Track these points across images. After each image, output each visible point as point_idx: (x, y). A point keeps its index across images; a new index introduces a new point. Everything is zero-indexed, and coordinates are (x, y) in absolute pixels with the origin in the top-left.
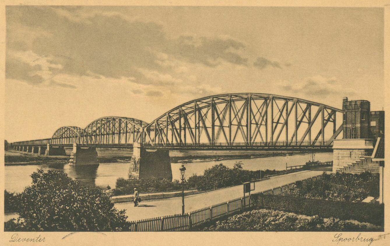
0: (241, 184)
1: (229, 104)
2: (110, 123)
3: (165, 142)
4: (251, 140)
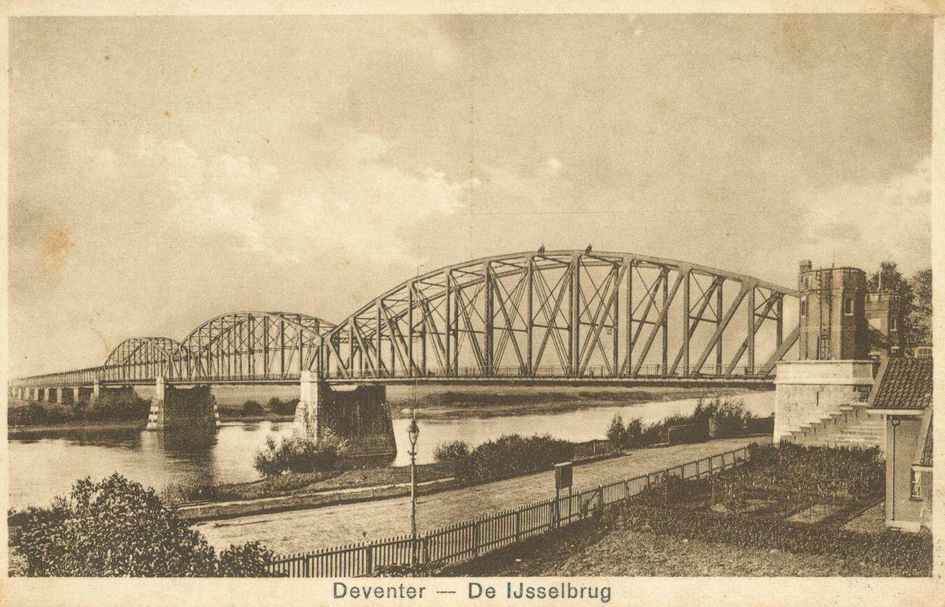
0: (549, 470)
1: (528, 276)
2: (243, 326)
3: (376, 367)
4: (578, 364)
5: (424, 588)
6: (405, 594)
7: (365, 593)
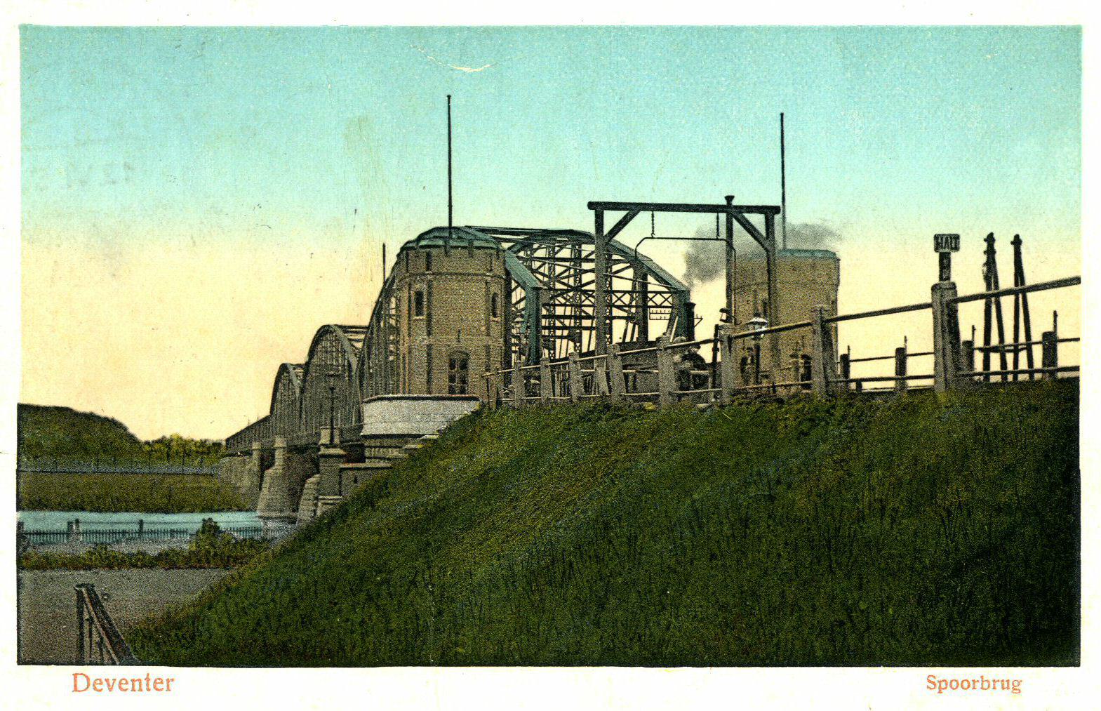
5: (172, 680)
6: (151, 686)
7: (109, 685)
